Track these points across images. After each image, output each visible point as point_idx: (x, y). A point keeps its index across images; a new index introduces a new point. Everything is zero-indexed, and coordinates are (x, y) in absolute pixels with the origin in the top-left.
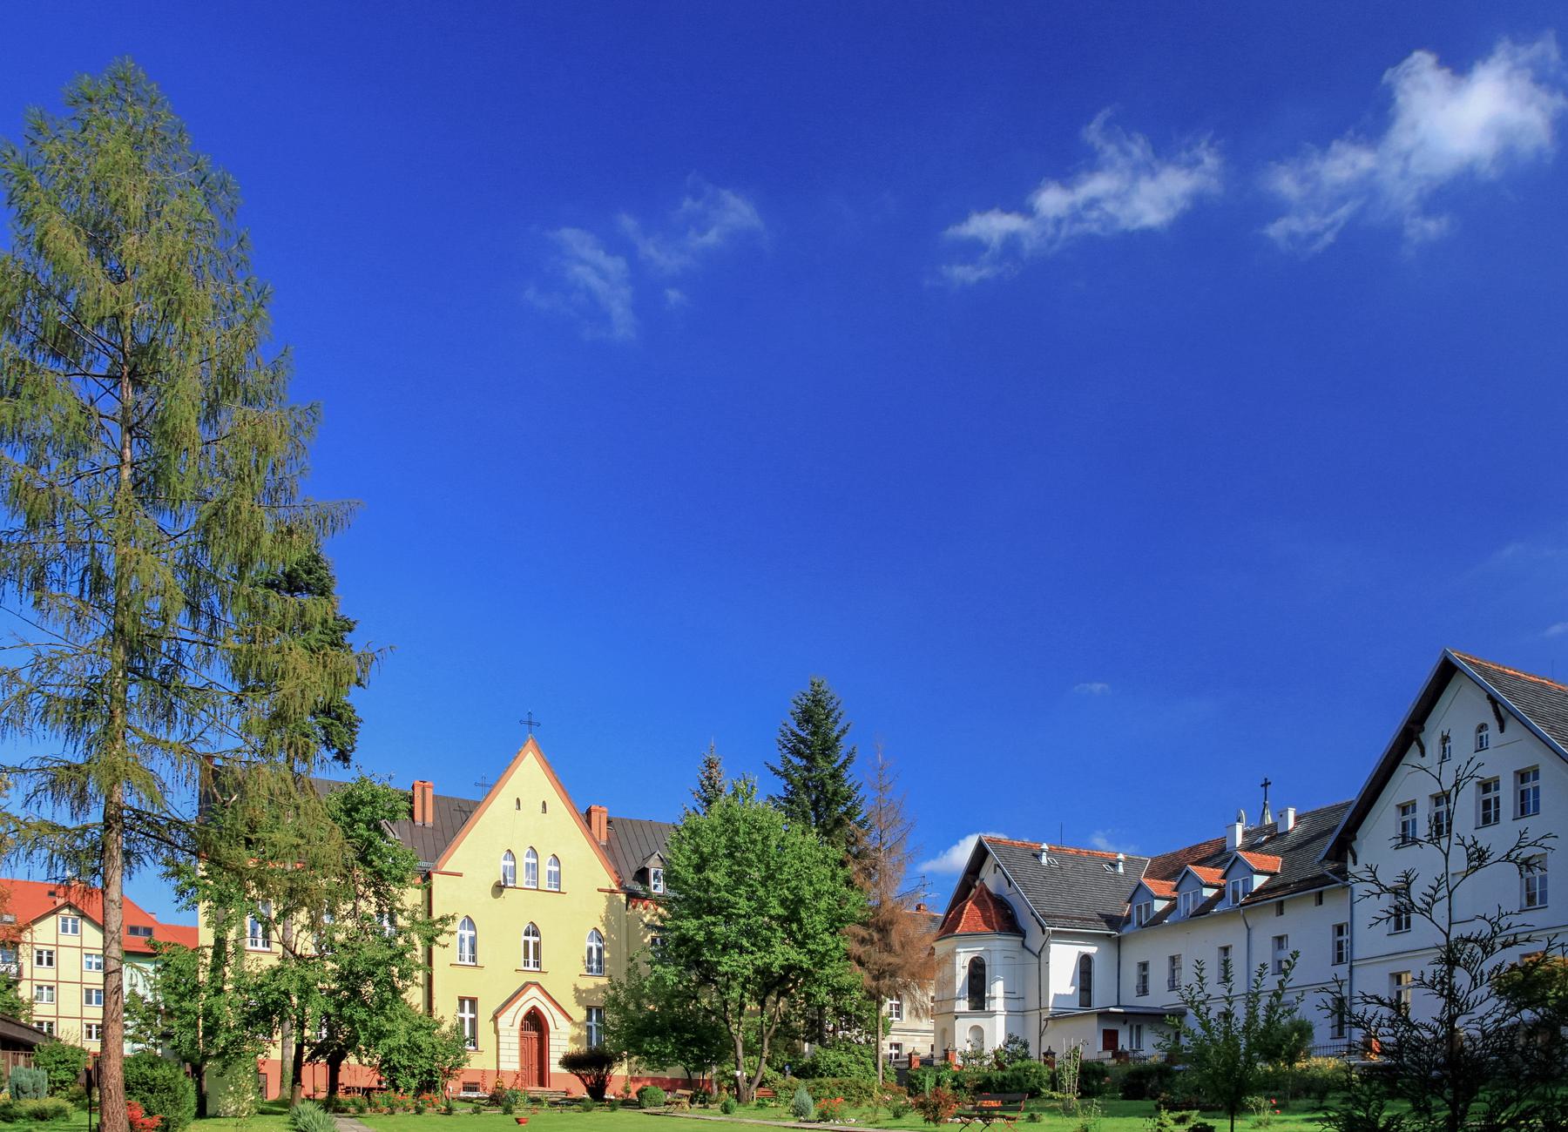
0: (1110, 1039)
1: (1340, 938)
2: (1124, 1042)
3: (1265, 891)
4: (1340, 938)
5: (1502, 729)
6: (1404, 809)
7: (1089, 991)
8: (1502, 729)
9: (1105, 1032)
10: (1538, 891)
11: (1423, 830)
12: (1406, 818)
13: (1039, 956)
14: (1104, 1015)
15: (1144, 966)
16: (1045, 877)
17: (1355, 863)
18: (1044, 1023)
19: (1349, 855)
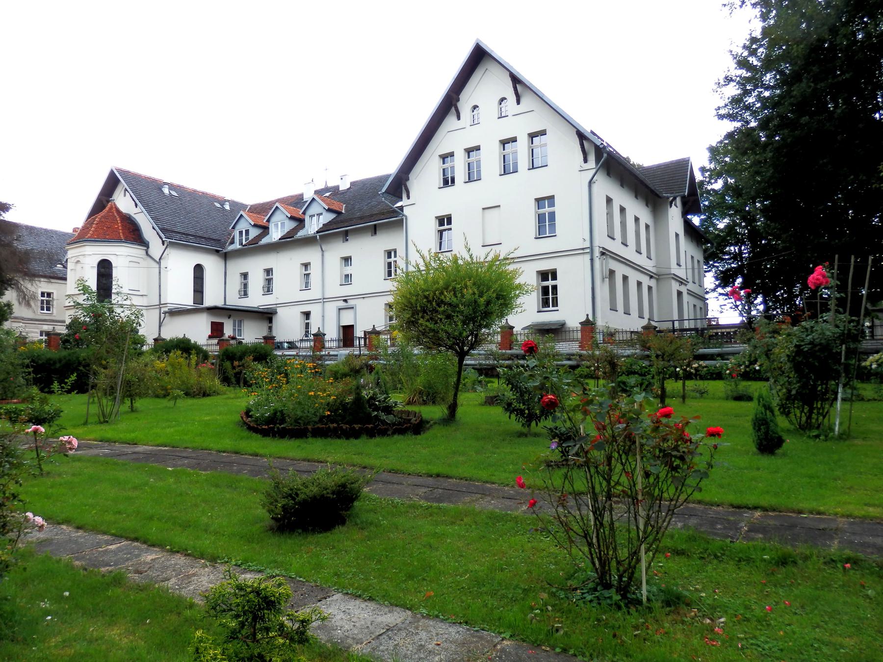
0: (217, 330)
1: (389, 260)
2: (228, 331)
3: (335, 223)
4: (389, 260)
5: (518, 102)
6: (444, 157)
7: (202, 292)
8: (518, 102)
9: (213, 323)
10: (547, 223)
11: (460, 175)
12: (445, 166)
13: (159, 263)
14: (213, 310)
15: (245, 276)
16: (166, 203)
17: (408, 198)
18: (163, 315)
19: (403, 188)
